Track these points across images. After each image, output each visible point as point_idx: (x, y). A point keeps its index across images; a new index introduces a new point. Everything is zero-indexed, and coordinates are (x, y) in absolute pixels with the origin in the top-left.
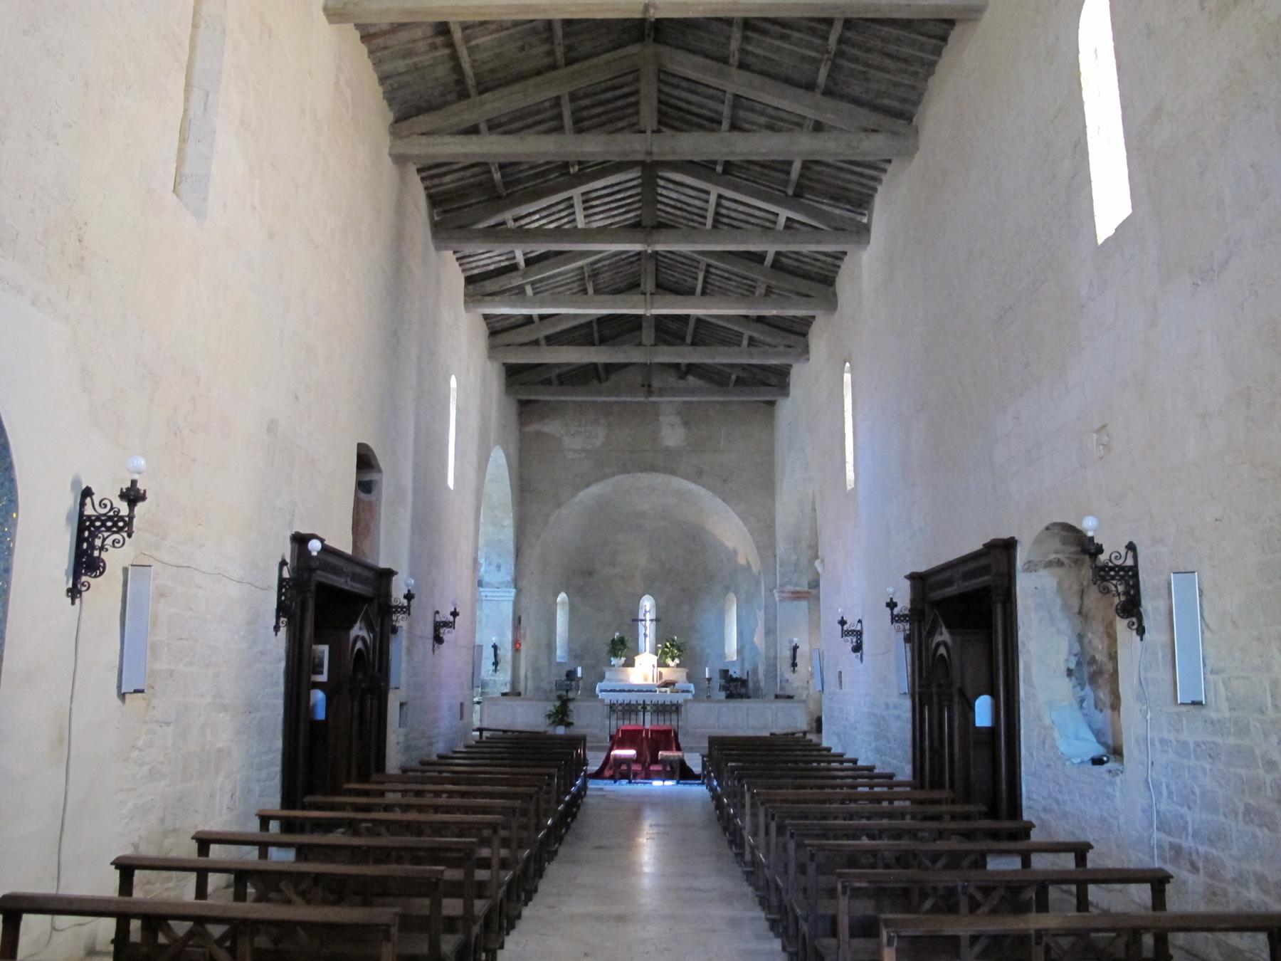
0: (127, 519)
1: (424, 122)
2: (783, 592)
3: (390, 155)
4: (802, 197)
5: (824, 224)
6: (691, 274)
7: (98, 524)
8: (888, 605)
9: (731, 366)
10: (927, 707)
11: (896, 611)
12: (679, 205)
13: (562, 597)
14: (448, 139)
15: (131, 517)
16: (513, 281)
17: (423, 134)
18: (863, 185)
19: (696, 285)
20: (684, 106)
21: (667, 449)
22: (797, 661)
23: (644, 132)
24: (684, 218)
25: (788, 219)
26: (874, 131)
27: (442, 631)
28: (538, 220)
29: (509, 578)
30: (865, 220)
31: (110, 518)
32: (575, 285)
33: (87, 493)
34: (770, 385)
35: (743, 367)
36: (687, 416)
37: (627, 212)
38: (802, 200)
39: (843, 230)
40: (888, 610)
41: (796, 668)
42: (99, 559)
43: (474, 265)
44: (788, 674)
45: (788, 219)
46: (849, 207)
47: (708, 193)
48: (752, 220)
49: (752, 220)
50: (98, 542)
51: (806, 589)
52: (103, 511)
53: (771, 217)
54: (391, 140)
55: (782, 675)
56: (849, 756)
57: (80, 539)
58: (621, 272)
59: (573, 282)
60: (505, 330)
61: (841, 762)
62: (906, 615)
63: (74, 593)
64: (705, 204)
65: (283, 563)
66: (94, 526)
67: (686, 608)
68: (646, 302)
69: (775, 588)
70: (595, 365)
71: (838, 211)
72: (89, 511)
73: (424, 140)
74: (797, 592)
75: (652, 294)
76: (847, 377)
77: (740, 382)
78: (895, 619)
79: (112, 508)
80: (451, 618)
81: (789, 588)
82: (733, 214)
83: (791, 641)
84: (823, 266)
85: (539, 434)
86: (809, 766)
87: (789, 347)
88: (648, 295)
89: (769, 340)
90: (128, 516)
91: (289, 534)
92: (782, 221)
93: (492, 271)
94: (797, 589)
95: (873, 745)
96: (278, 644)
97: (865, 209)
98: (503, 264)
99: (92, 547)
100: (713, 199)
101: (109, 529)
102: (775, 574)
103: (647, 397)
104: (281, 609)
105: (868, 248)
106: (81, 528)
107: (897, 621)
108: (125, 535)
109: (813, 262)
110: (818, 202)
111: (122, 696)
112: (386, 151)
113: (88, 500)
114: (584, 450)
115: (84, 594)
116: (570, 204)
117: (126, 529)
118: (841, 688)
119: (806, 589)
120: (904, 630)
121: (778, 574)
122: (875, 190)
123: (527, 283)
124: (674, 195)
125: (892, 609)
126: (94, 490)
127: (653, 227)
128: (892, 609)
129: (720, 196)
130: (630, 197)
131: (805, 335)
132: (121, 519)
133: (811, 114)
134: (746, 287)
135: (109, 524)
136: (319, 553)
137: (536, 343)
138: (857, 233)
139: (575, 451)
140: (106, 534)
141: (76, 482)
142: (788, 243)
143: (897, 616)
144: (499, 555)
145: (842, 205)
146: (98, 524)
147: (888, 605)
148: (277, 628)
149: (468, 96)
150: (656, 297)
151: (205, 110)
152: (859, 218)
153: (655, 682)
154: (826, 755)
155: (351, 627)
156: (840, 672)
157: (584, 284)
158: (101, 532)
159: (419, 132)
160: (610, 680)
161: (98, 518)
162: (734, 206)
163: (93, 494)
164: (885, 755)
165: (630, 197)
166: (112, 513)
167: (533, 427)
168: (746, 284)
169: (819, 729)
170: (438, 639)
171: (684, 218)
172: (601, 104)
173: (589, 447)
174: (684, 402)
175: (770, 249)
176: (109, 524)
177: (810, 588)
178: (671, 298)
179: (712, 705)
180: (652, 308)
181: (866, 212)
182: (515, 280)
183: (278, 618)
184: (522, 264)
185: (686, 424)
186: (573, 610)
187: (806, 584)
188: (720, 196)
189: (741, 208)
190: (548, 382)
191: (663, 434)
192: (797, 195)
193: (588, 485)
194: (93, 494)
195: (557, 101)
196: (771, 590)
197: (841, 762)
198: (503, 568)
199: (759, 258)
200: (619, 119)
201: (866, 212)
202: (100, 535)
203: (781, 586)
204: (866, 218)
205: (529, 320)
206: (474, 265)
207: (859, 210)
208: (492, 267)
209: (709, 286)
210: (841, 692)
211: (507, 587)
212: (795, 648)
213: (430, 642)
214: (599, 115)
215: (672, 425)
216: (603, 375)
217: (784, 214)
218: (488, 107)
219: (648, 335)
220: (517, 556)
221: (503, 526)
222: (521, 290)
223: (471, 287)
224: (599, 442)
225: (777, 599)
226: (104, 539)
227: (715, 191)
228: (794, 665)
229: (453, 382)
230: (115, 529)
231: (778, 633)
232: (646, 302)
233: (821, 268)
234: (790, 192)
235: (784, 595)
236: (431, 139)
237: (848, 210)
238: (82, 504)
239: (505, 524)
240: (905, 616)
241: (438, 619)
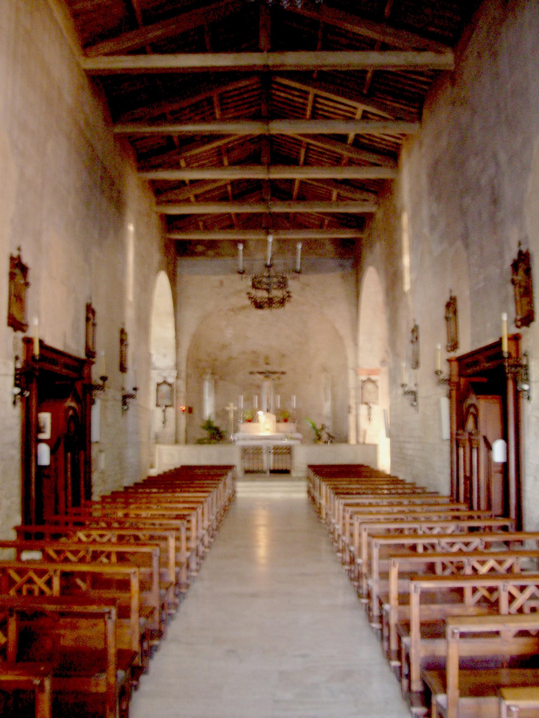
25: (364, 112)
45: (364, 112)
47: (307, 93)
82: (326, 108)
100: (311, 97)
116: (210, 101)
129: (316, 96)
148: (14, 403)
160: (243, 432)
188: (316, 96)
189: (331, 104)
199: (342, 138)
217: (361, 107)
227: (312, 91)
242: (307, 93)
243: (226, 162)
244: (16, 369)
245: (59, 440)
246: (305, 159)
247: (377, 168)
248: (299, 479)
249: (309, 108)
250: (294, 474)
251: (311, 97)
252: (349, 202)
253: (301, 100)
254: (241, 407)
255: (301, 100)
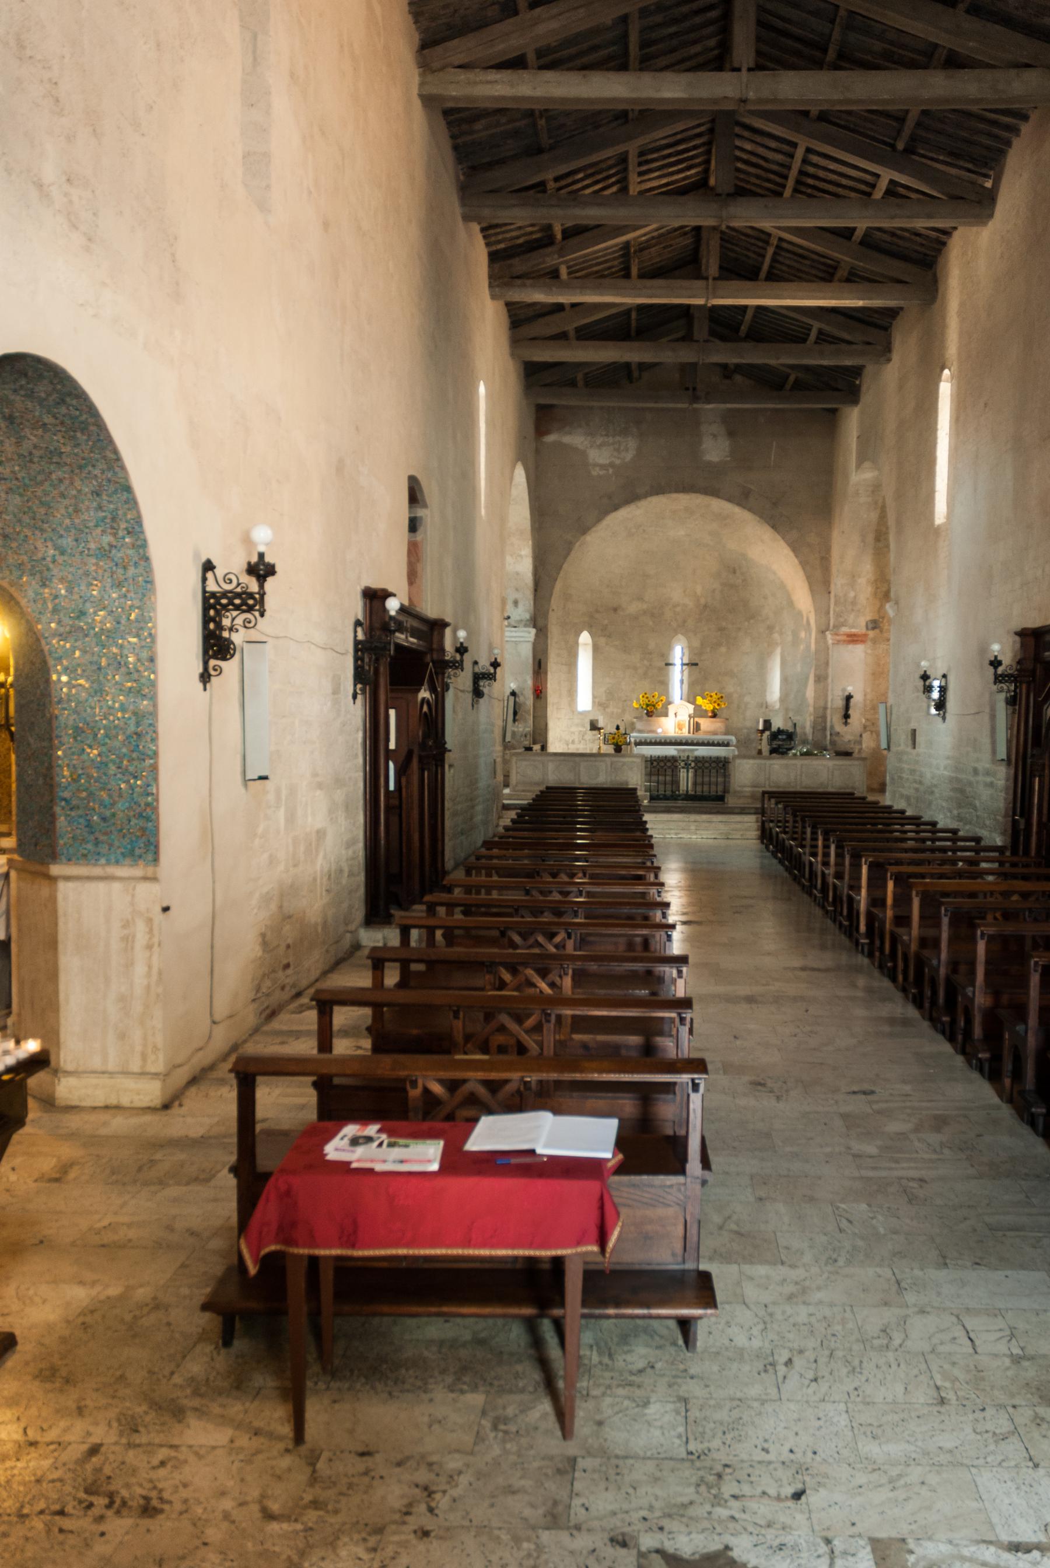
0: (257, 596)
1: (460, 49)
2: (837, 634)
3: (421, 96)
4: (913, 153)
5: (939, 192)
6: (757, 250)
7: (224, 601)
8: (992, 663)
9: (793, 367)
10: (1037, 779)
11: (1000, 670)
12: (754, 159)
13: (585, 638)
14: (493, 75)
15: (262, 595)
16: (548, 259)
17: (460, 67)
18: (996, 137)
19: (762, 263)
20: (779, 24)
21: (710, 464)
22: (850, 712)
23: (739, 70)
24: (758, 177)
25: (891, 181)
26: (1028, 66)
27: (481, 683)
28: (582, 180)
29: (527, 616)
30: (988, 184)
31: (238, 595)
32: (616, 263)
33: (208, 566)
34: (837, 390)
35: (807, 368)
36: (733, 424)
37: (688, 168)
38: (914, 157)
39: (962, 198)
40: (991, 669)
41: (849, 721)
42: (229, 642)
43: (500, 237)
44: (839, 727)
45: (891, 181)
46: (970, 166)
47: (794, 145)
48: (844, 181)
49: (844, 181)
50: (226, 622)
51: (864, 631)
52: (228, 587)
53: (868, 178)
54: (420, 75)
55: (832, 727)
56: (926, 818)
57: (206, 620)
58: (671, 246)
59: (614, 259)
60: (530, 320)
61: (918, 825)
62: (1012, 675)
63: (205, 677)
64: (789, 160)
65: (358, 623)
66: (220, 604)
67: (723, 649)
68: (707, 288)
69: (827, 629)
70: (627, 366)
71: (954, 171)
72: (212, 587)
73: (463, 76)
74: (854, 635)
75: (714, 279)
76: (946, 389)
77: (798, 385)
78: (998, 679)
79: (239, 584)
80: (492, 670)
81: (845, 630)
82: (821, 174)
83: (844, 690)
84: (924, 242)
85: (559, 445)
86: (888, 828)
87: (869, 343)
88: (710, 281)
89: (846, 336)
90: (258, 593)
91: (359, 590)
92: (883, 185)
93: (520, 245)
94: (853, 630)
95: (955, 812)
96: (356, 713)
97: (991, 169)
98: (534, 237)
99: (220, 627)
100: (800, 153)
101: (237, 608)
102: (828, 613)
103: (691, 404)
104: (360, 676)
105: (990, 224)
106: (206, 606)
107: (1000, 682)
108: (257, 614)
109: (913, 237)
110: (932, 159)
111: (246, 781)
112: (415, 91)
113: (209, 575)
114: (612, 465)
115: (213, 679)
116: (623, 159)
117: (257, 607)
118: (914, 748)
119: (864, 631)
120: (1009, 691)
121: (832, 612)
122: (1009, 144)
123: (562, 263)
124: (748, 146)
125: (996, 668)
126: (215, 563)
127: (728, 195)
128: (996, 668)
129: (809, 150)
130: (695, 148)
131: (886, 329)
132: (251, 596)
133: (945, 40)
134: (821, 267)
135: (237, 601)
136: (397, 612)
137: (563, 336)
138: (979, 202)
139: (602, 467)
140: (235, 613)
141: (197, 555)
142: (893, 217)
143: (1001, 675)
144: (517, 590)
145: (961, 163)
146: (224, 601)
147: (992, 663)
148: (355, 697)
149: (516, 13)
150: (719, 282)
151: (255, 59)
152: (980, 180)
153: (691, 735)
154: (892, 816)
155: (419, 690)
156: (914, 731)
157: (629, 261)
158: (228, 611)
159: (457, 63)
161: (224, 594)
162: (823, 162)
163: (214, 567)
164: (970, 823)
165: (695, 148)
166: (239, 590)
167: (551, 438)
168: (824, 264)
169: (882, 789)
170: (478, 693)
171: (758, 177)
172: (675, 21)
173: (618, 462)
174: (729, 410)
175: (861, 222)
176: (237, 601)
177: (867, 628)
178: (736, 284)
179: (763, 762)
180: (715, 297)
181: (991, 173)
182: (550, 259)
183: (355, 685)
184: (559, 236)
185: (731, 434)
186: (596, 649)
187: (863, 624)
188: (809, 150)
189: (833, 166)
190: (573, 384)
191: (704, 446)
192: (909, 150)
193: (616, 508)
194: (214, 567)
195: (624, 19)
196: (823, 632)
197: (918, 825)
198: (520, 605)
199: (847, 233)
200: (695, 42)
201: (991, 173)
202: (228, 614)
203: (834, 627)
204: (991, 181)
205: (559, 308)
206: (500, 237)
207: (984, 171)
208: (521, 241)
209: (778, 265)
210: (914, 752)
211: (526, 626)
212: (849, 698)
213: (469, 697)
214: (671, 36)
215: (715, 436)
216: (636, 374)
217: (887, 175)
218: (541, 29)
219: (701, 330)
220: (536, 590)
221: (521, 556)
222: (554, 274)
223: (497, 266)
224: (629, 456)
225: (830, 642)
226: (233, 619)
227: (803, 143)
228: (846, 716)
229: (482, 389)
230: (244, 607)
231: (830, 680)
232: (707, 288)
233: (922, 245)
234: (900, 146)
235: (838, 638)
236: (470, 75)
237: (969, 171)
238: (204, 579)
239: (523, 553)
240: (1010, 676)
241: (477, 670)
242: (794, 145)
243: (634, 271)
244: (357, 643)
245: (410, 754)
246: (771, 267)
247: (899, 286)
248: (742, 811)
249: (793, 174)
250: (731, 801)
251: (800, 153)
252: (844, 347)
253: (779, 157)
254: (805, 734)
255: (779, 157)
